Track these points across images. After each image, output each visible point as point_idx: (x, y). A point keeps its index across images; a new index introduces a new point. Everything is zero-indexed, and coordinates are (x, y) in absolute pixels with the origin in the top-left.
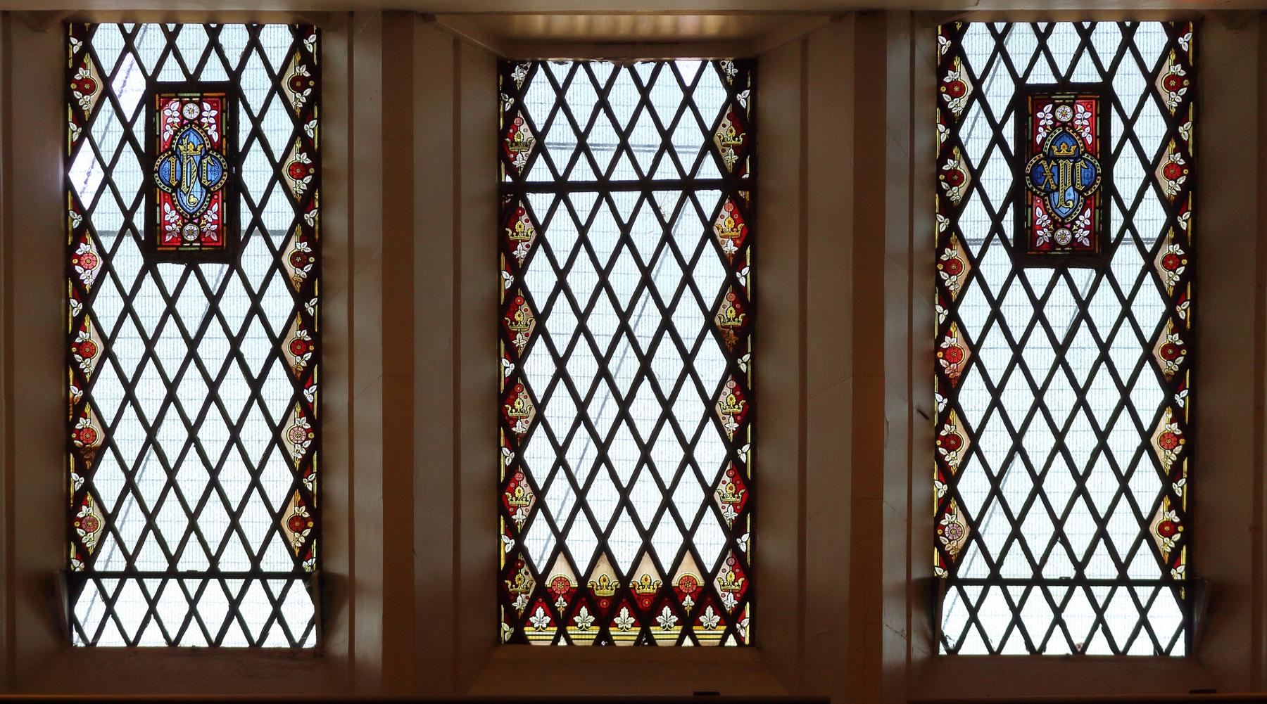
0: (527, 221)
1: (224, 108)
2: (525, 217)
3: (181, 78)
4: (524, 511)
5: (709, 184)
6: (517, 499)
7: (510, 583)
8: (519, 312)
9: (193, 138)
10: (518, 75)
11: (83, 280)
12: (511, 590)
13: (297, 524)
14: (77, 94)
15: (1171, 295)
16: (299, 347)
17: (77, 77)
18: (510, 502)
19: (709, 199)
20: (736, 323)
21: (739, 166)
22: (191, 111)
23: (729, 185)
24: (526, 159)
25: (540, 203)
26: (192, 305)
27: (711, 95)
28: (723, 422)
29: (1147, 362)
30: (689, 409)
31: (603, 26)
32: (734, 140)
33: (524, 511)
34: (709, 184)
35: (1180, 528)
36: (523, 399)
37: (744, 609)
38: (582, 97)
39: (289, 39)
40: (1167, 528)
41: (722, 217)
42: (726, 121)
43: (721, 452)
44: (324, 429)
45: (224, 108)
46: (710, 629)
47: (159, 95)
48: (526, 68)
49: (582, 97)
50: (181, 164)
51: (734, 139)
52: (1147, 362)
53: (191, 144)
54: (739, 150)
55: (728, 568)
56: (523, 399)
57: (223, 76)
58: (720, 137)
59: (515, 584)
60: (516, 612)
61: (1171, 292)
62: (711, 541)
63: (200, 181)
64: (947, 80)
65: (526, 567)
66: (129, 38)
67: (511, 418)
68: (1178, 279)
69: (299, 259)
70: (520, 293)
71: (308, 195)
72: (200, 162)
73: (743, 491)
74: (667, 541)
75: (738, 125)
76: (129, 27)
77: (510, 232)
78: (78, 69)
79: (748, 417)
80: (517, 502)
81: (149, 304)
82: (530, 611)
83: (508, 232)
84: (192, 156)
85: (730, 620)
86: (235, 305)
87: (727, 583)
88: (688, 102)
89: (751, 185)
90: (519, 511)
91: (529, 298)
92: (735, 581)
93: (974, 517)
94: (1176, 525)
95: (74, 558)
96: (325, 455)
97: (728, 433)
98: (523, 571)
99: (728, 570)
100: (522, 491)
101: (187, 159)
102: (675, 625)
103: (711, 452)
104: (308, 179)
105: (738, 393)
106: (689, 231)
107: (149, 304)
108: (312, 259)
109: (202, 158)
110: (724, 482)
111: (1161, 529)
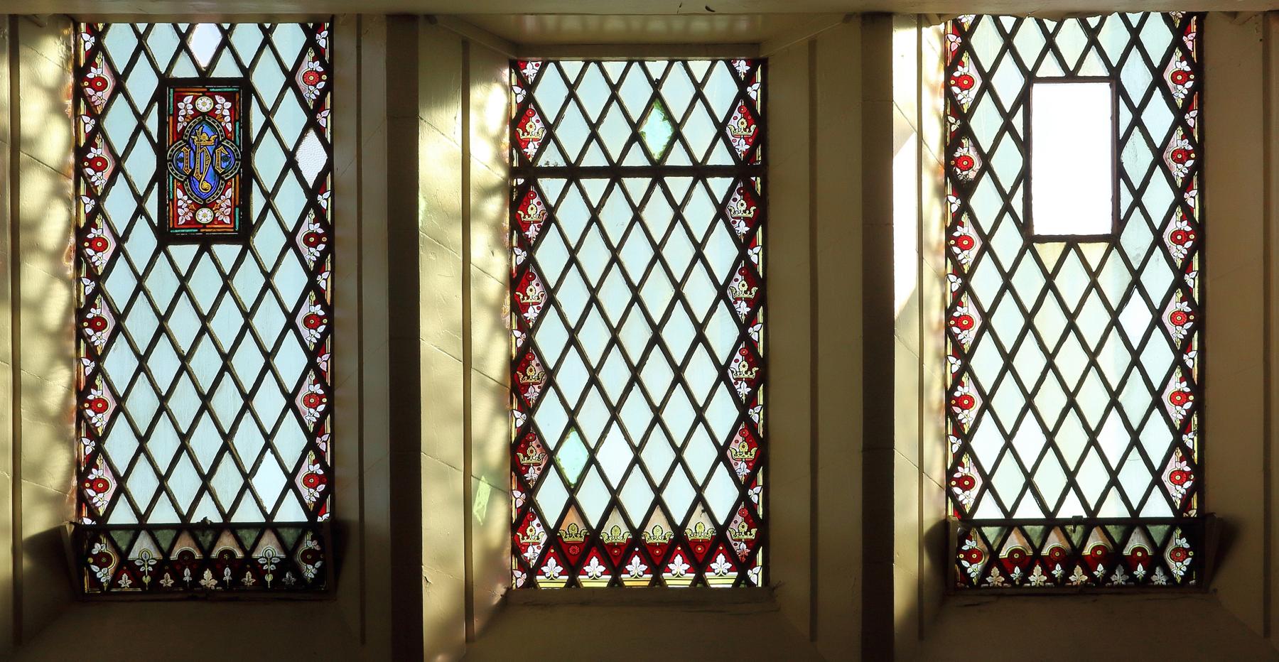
0: (538, 121)
1: (237, 118)
2: (537, 521)
3: (193, 74)
4: (536, 470)
5: (720, 171)
6: (528, 537)
7: (521, 132)
8: (530, 123)
9: (207, 129)
10: (530, 70)
11: (100, 579)
12: (522, 542)
13: (312, 321)
14: (90, 91)
15: (1181, 106)
16: (311, 78)
17: (90, 76)
18: (522, 542)
19: (720, 186)
20: (749, 537)
21: (750, 154)
22: (204, 104)
23: (741, 171)
24: (537, 147)
25: (551, 187)
26: (205, 284)
27: (722, 89)
28: (736, 468)
29: (1157, 89)
30: (701, 374)
31: (614, 26)
32: (746, 131)
33: (536, 470)
34: (720, 171)
35: (1193, 155)
36: (536, 448)
37: (754, 76)
38: (593, 92)
39: (302, 38)
40: (1178, 398)
41: (736, 118)
42: (738, 518)
43: (732, 493)
44: (336, 72)
45: (237, 118)
46: (721, 575)
47: (170, 229)
48: (537, 65)
49: (593, 92)
50: (195, 153)
51: (746, 533)
52: (1157, 89)
53: (205, 137)
54: (751, 303)
55: (739, 116)
56: (536, 448)
57: (236, 73)
58: (730, 210)
59: (527, 375)
60: (528, 239)
61: (1181, 104)
62: (722, 496)
63: (214, 168)
64: (956, 74)
65: (537, 117)
66: (142, 38)
67: (522, 545)
68: (1185, 333)
69: (312, 481)
70: (531, 106)
71: (320, 345)
72: (214, 152)
73: (754, 208)
74: (679, 497)
75: (751, 360)
76: (142, 27)
77: (521, 296)
78: (91, 229)
79: (761, 462)
80: (529, 136)
81: (162, 284)
82: (542, 560)
83: (520, 215)
84: (206, 146)
85: (741, 565)
86: (248, 282)
87: (741, 533)
88: (700, 338)
89: (763, 171)
90: (531, 145)
91: (539, 514)
92: (747, 209)
93: (986, 150)
94: (1188, 233)
95: (84, 195)
96: (337, 497)
97: (739, 153)
98: (534, 283)
99: (739, 118)
100: (534, 290)
101: (201, 148)
102: (686, 572)
103: (723, 333)
104: (321, 247)
105: (751, 360)
106: (700, 212)
107: (162, 284)
108: (325, 321)
109: (216, 148)
110: (737, 361)
111: (1172, 398)
